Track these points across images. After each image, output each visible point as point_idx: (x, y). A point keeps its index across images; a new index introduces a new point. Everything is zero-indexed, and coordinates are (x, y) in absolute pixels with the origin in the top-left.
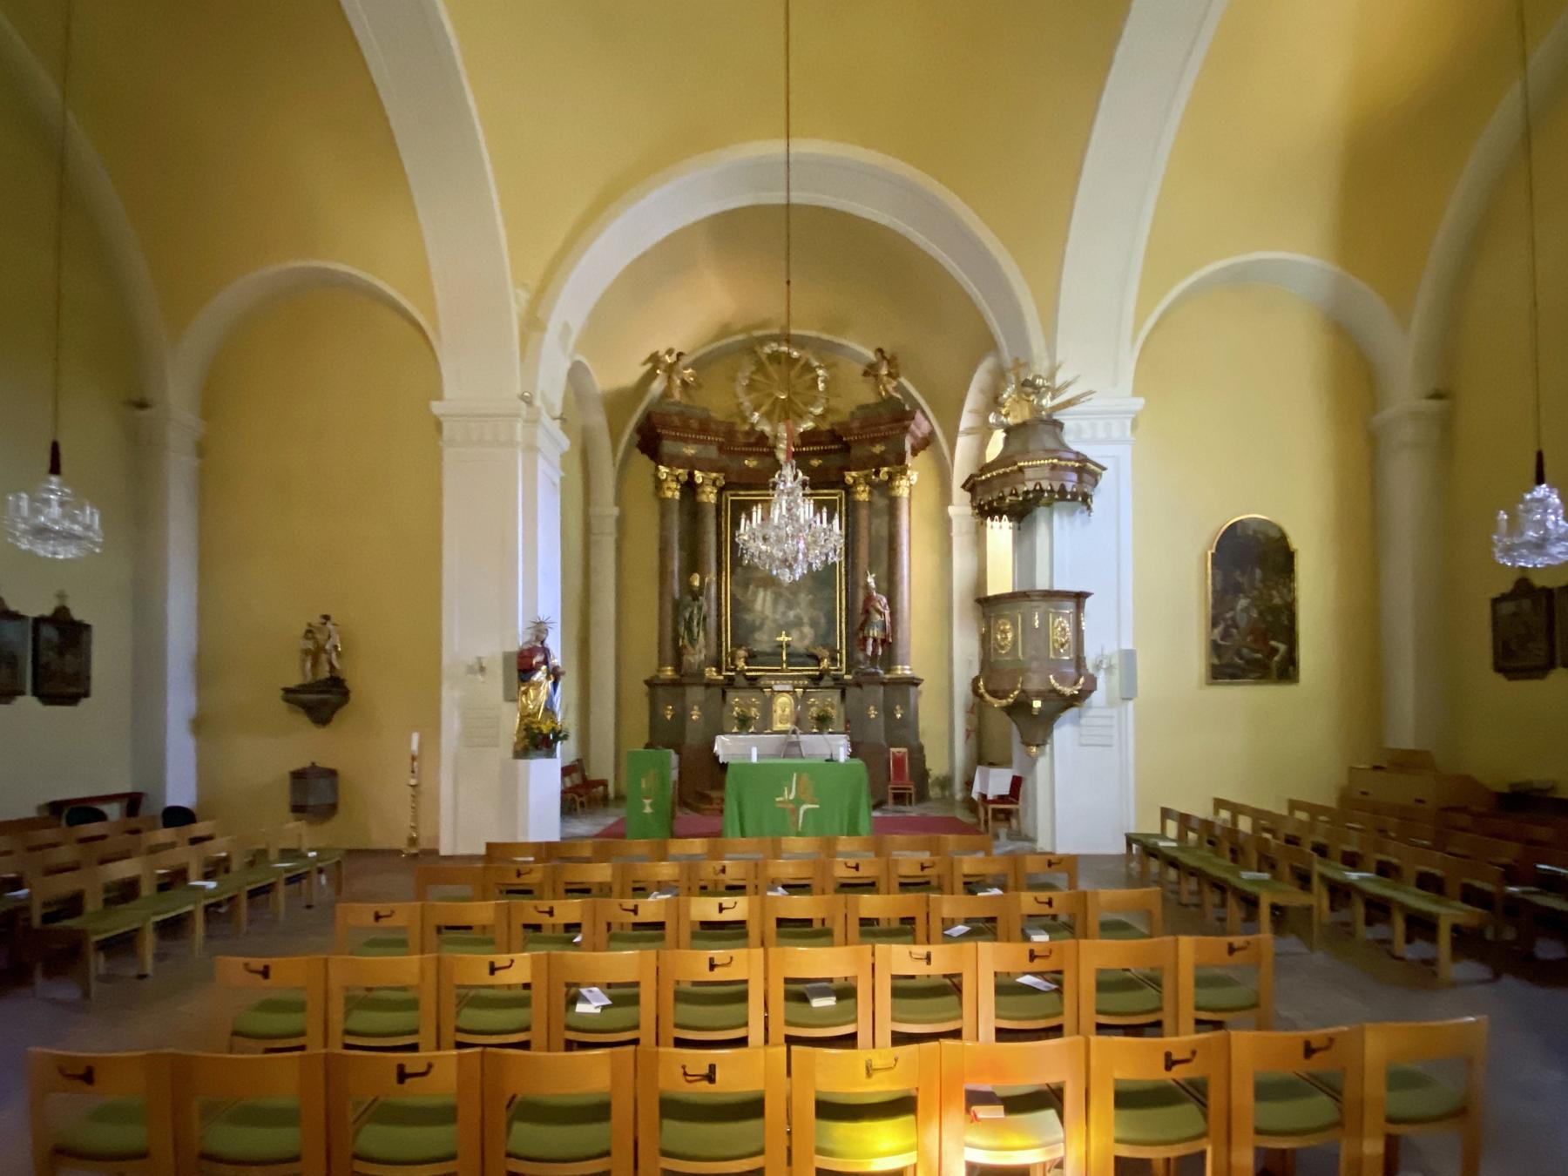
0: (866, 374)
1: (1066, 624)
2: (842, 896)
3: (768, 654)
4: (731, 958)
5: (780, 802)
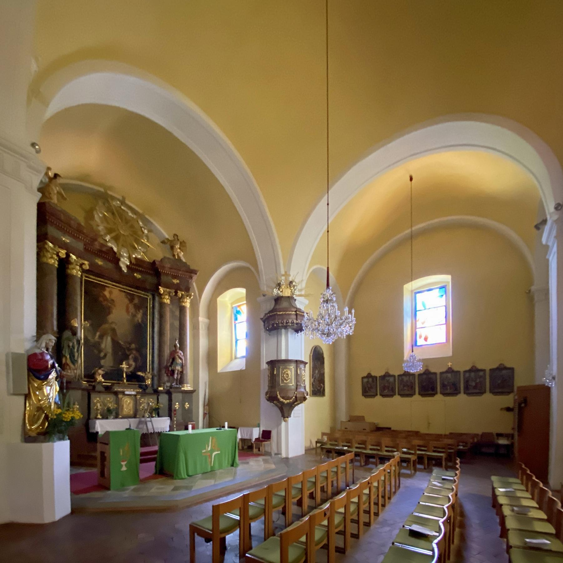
5: (204, 452)
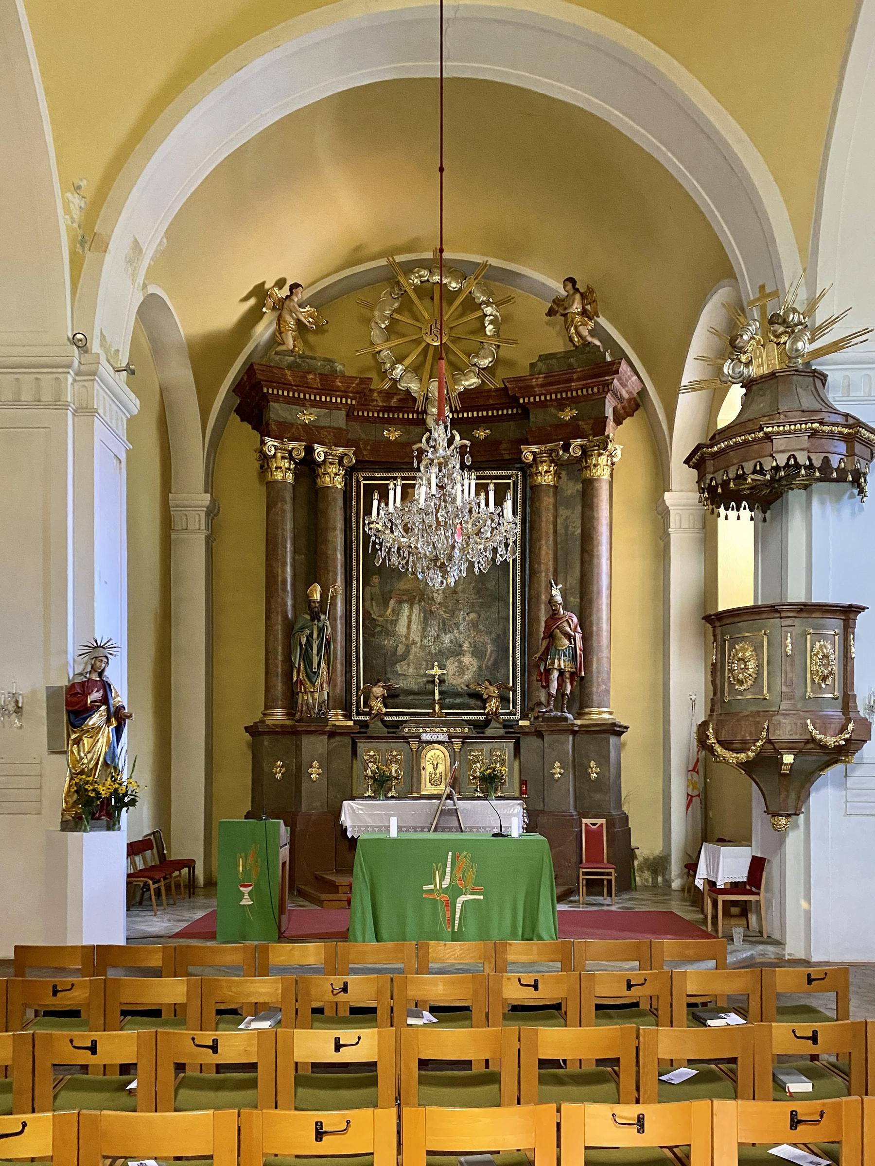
0: (551, 313)
1: (829, 649)
2: (513, 1028)
3: (411, 692)
4: (348, 1122)
